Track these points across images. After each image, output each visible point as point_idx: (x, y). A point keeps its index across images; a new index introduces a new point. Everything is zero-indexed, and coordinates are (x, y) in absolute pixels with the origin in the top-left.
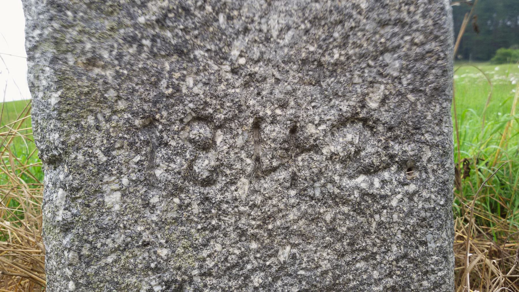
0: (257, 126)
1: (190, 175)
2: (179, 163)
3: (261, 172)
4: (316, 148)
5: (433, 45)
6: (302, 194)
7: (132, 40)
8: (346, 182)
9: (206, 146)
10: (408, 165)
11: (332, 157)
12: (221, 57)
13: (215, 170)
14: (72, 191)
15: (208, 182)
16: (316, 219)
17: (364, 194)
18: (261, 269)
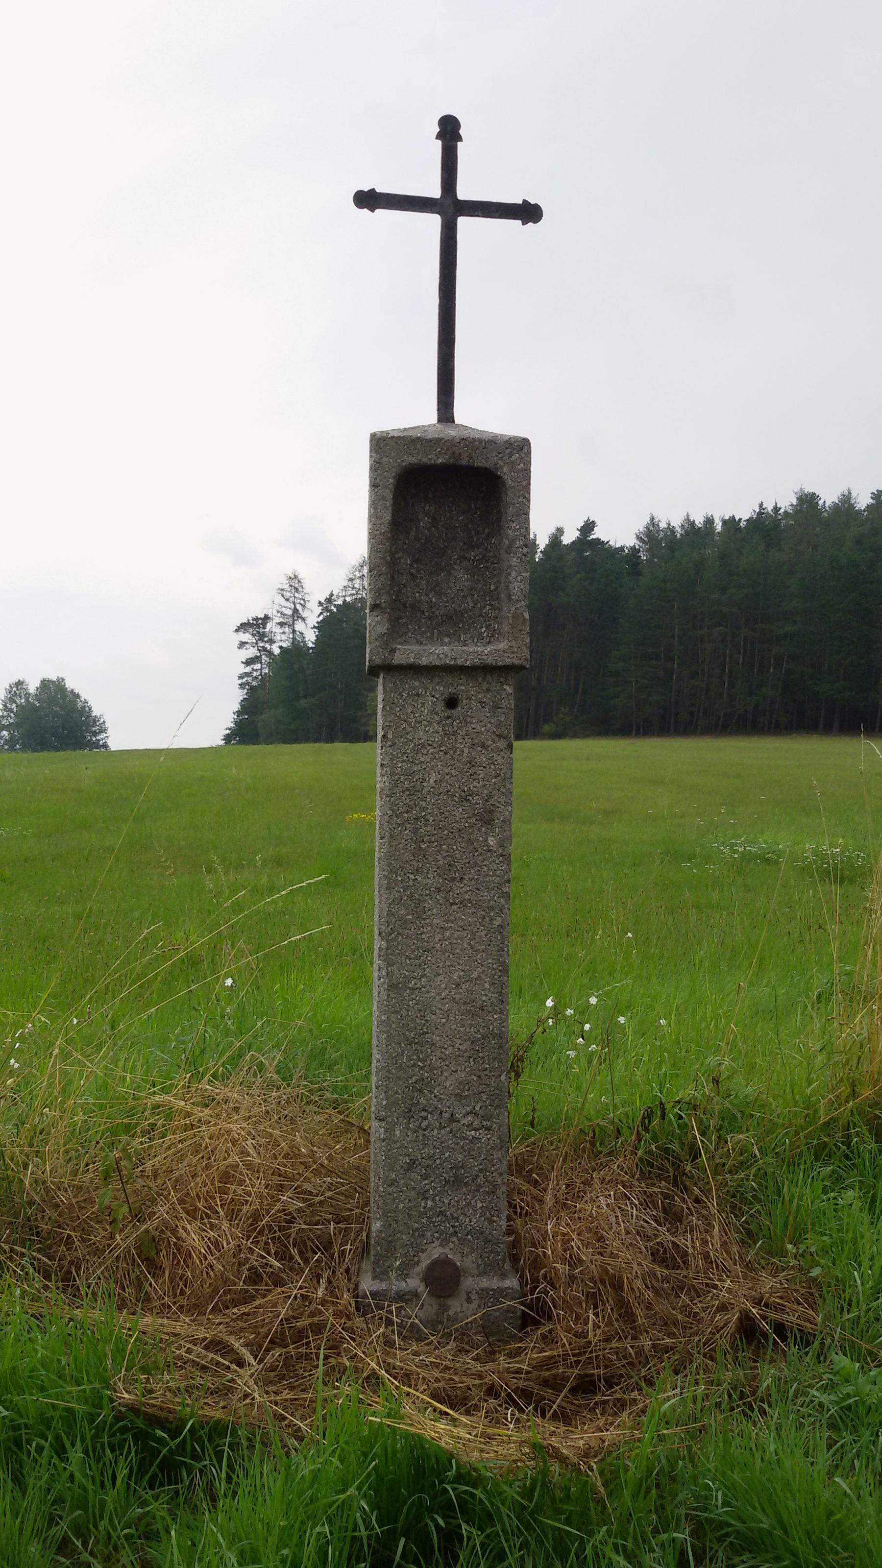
0: (441, 1113)
1: (420, 1127)
2: (417, 1123)
3: (441, 1128)
4: (458, 1121)
5: (497, 1092)
6: (454, 1135)
7: (408, 1087)
8: (468, 1133)
9: (425, 1118)
10: (488, 1129)
11: (464, 1124)
12: (431, 1092)
13: (427, 1126)
14: (386, 1130)
15: (425, 1130)
16: (457, 1144)
17: (473, 1137)
18: (440, 1158)
